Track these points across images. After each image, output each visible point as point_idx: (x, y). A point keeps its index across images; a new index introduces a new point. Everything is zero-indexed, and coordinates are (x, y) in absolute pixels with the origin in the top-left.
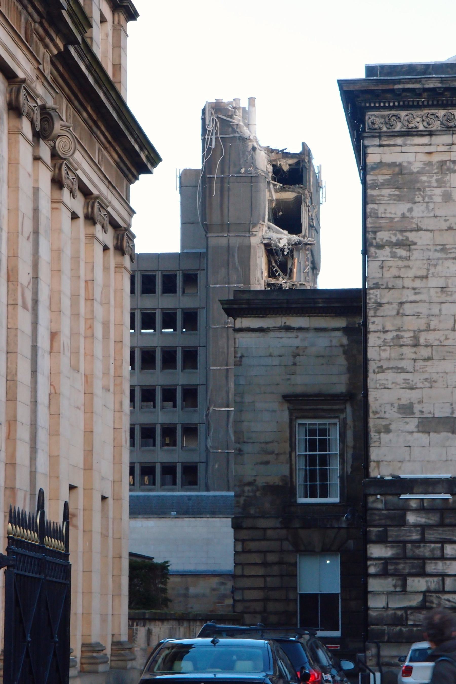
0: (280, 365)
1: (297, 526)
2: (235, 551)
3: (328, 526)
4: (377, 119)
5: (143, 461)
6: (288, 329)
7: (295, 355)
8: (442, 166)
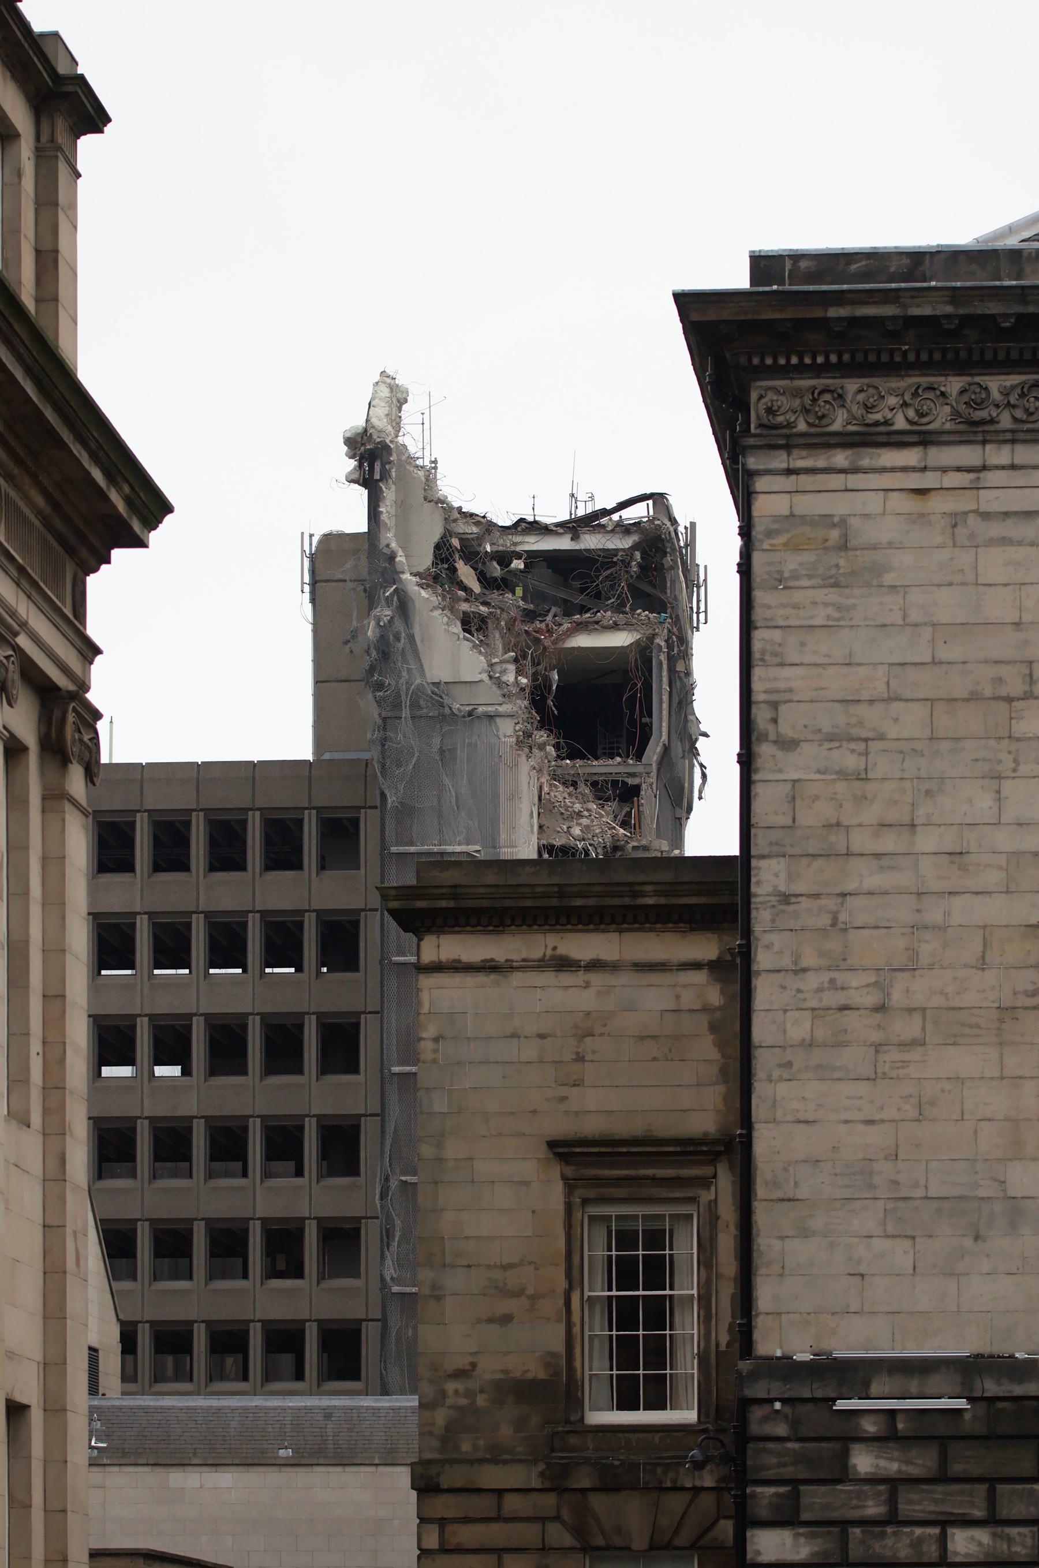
0: (541, 1061)
1: (586, 1484)
2: (419, 1549)
3: (669, 1484)
4: (783, 399)
5: (214, 1318)
6: (563, 964)
7: (583, 1034)
8: (955, 525)
